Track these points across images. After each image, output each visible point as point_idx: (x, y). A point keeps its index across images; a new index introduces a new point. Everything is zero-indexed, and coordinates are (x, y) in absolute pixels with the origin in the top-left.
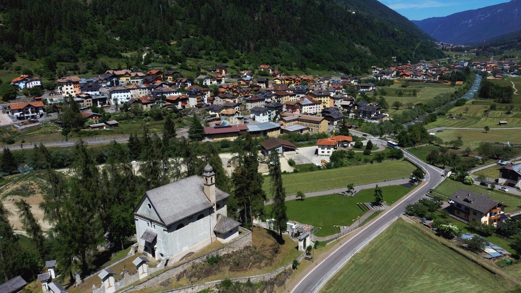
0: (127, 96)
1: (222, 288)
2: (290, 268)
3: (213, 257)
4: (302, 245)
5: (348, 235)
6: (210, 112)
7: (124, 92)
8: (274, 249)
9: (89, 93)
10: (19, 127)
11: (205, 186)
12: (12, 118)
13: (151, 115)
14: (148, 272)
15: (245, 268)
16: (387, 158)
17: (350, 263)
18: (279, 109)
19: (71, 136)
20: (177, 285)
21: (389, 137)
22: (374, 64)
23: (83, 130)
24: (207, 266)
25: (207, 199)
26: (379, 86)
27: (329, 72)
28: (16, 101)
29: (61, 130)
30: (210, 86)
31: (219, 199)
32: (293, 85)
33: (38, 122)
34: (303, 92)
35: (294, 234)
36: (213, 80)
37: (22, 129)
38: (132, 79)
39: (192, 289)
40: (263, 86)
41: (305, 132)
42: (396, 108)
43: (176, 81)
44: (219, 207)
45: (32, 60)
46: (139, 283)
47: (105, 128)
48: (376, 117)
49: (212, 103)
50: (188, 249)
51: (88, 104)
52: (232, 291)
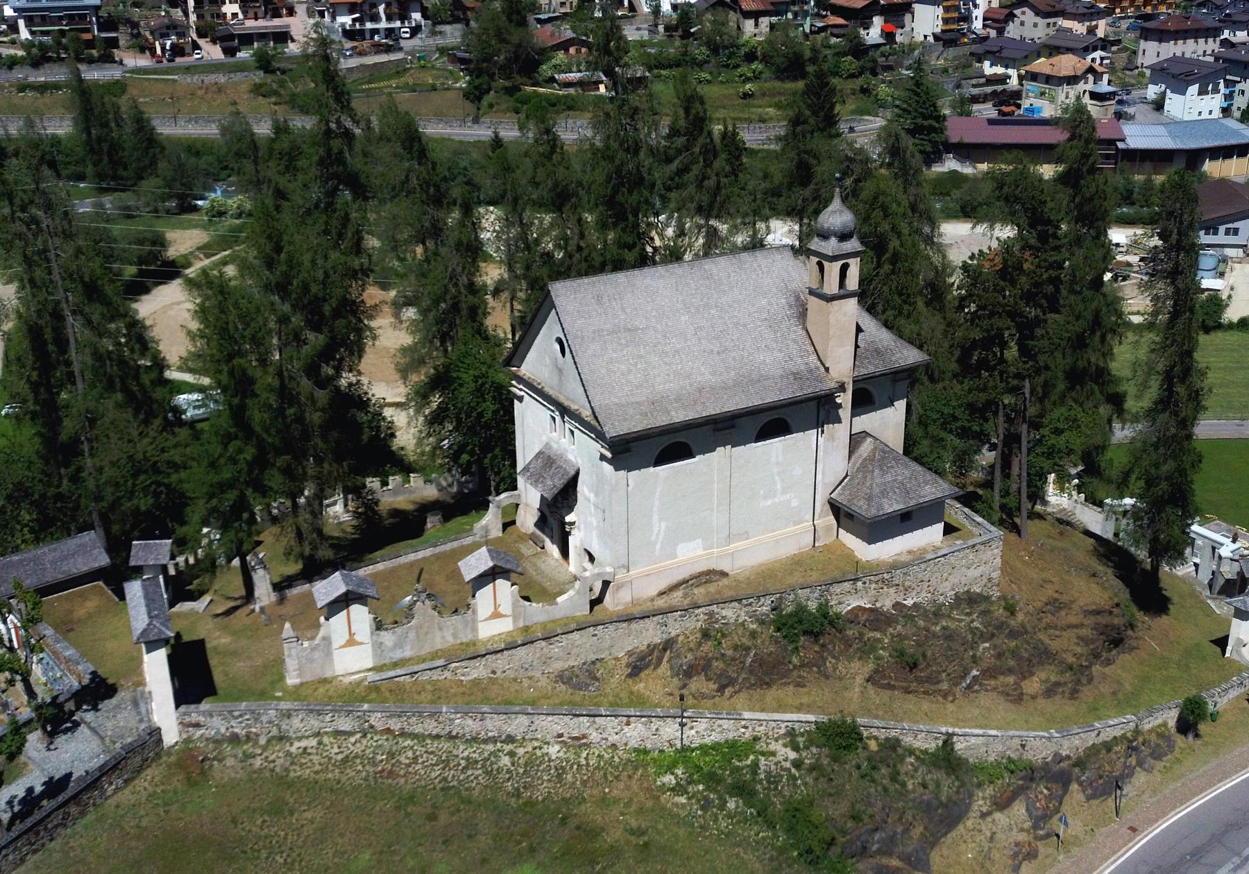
1: (814, 750)
2: (1165, 724)
6: (987, 64)
8: (1103, 630)
11: (813, 299)
13: (766, 59)
14: (515, 617)
15: (945, 686)
19: (491, 106)
23: (529, 89)
24: (767, 644)
25: (813, 358)
31: (869, 369)
33: (401, 49)
35: (1220, 582)
39: (682, 725)
44: (864, 400)
46: (471, 651)
49: (1000, 31)
50: (700, 552)
52: (855, 774)
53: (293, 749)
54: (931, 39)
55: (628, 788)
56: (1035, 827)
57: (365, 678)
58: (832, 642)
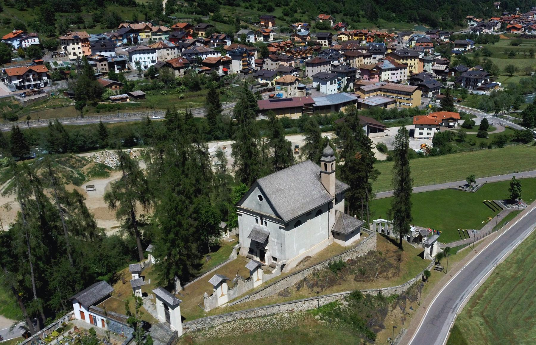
0: (151, 58)
1: (352, 301)
2: (420, 279)
3: (335, 263)
4: (429, 252)
5: (483, 241)
6: (259, 79)
7: (148, 53)
9: (103, 54)
10: (21, 99)
12: (11, 87)
13: (185, 84)
14: (263, 279)
15: (372, 278)
16: (511, 141)
17: (494, 275)
18: (351, 75)
19: (87, 111)
20: (298, 296)
21: (507, 114)
22: (470, 12)
25: (325, 191)
26: (480, 43)
27: (409, 24)
28: (12, 64)
29: (73, 103)
30: (256, 44)
32: (364, 42)
33: (44, 92)
34: (381, 51)
36: (258, 36)
37: (25, 102)
38: (153, 35)
39: (318, 301)
40: (325, 43)
41: (390, 107)
42: (509, 74)
43: (212, 38)
45: (22, 10)
47: (128, 100)
48: (484, 86)
49: (261, 67)
50: (304, 252)
51: (103, 69)
53: (216, 330)
54: (239, 72)
55: (308, 321)
56: (403, 312)
57: (228, 305)
58: (344, 271)
